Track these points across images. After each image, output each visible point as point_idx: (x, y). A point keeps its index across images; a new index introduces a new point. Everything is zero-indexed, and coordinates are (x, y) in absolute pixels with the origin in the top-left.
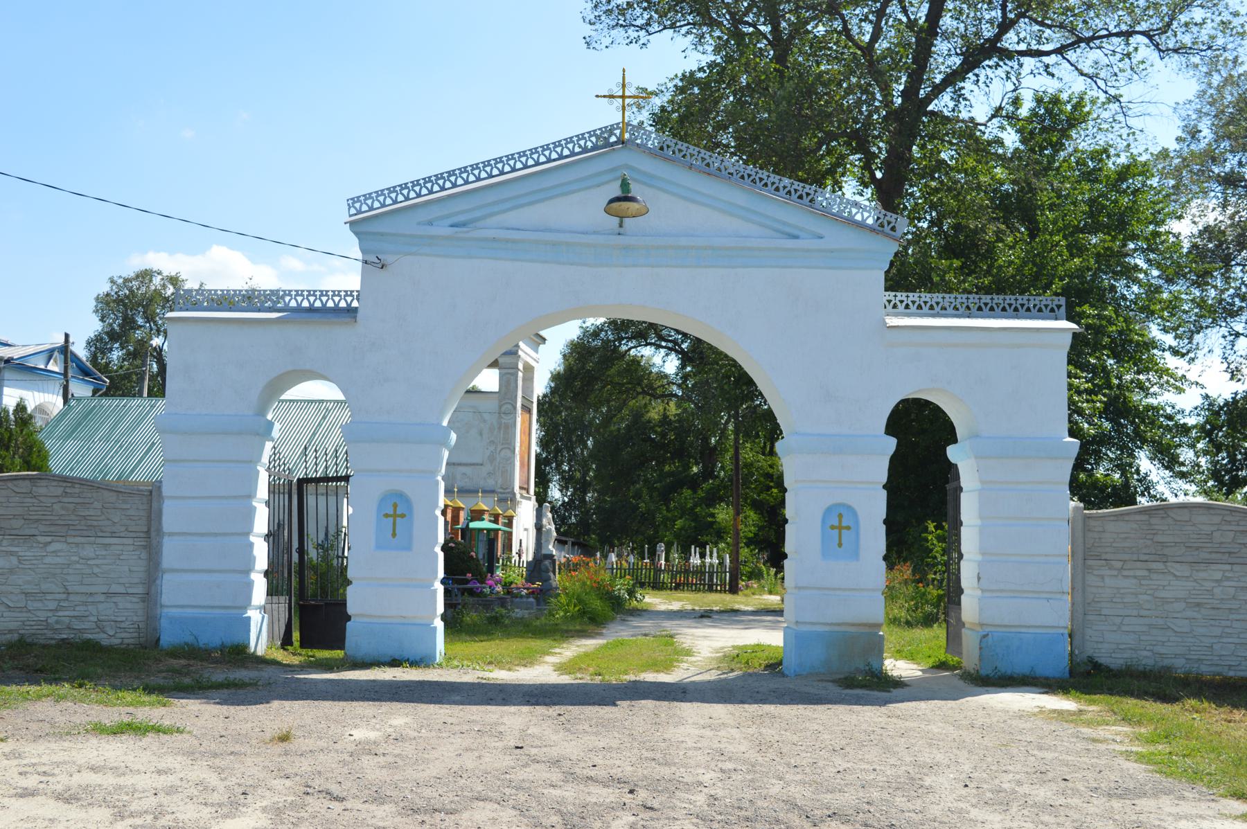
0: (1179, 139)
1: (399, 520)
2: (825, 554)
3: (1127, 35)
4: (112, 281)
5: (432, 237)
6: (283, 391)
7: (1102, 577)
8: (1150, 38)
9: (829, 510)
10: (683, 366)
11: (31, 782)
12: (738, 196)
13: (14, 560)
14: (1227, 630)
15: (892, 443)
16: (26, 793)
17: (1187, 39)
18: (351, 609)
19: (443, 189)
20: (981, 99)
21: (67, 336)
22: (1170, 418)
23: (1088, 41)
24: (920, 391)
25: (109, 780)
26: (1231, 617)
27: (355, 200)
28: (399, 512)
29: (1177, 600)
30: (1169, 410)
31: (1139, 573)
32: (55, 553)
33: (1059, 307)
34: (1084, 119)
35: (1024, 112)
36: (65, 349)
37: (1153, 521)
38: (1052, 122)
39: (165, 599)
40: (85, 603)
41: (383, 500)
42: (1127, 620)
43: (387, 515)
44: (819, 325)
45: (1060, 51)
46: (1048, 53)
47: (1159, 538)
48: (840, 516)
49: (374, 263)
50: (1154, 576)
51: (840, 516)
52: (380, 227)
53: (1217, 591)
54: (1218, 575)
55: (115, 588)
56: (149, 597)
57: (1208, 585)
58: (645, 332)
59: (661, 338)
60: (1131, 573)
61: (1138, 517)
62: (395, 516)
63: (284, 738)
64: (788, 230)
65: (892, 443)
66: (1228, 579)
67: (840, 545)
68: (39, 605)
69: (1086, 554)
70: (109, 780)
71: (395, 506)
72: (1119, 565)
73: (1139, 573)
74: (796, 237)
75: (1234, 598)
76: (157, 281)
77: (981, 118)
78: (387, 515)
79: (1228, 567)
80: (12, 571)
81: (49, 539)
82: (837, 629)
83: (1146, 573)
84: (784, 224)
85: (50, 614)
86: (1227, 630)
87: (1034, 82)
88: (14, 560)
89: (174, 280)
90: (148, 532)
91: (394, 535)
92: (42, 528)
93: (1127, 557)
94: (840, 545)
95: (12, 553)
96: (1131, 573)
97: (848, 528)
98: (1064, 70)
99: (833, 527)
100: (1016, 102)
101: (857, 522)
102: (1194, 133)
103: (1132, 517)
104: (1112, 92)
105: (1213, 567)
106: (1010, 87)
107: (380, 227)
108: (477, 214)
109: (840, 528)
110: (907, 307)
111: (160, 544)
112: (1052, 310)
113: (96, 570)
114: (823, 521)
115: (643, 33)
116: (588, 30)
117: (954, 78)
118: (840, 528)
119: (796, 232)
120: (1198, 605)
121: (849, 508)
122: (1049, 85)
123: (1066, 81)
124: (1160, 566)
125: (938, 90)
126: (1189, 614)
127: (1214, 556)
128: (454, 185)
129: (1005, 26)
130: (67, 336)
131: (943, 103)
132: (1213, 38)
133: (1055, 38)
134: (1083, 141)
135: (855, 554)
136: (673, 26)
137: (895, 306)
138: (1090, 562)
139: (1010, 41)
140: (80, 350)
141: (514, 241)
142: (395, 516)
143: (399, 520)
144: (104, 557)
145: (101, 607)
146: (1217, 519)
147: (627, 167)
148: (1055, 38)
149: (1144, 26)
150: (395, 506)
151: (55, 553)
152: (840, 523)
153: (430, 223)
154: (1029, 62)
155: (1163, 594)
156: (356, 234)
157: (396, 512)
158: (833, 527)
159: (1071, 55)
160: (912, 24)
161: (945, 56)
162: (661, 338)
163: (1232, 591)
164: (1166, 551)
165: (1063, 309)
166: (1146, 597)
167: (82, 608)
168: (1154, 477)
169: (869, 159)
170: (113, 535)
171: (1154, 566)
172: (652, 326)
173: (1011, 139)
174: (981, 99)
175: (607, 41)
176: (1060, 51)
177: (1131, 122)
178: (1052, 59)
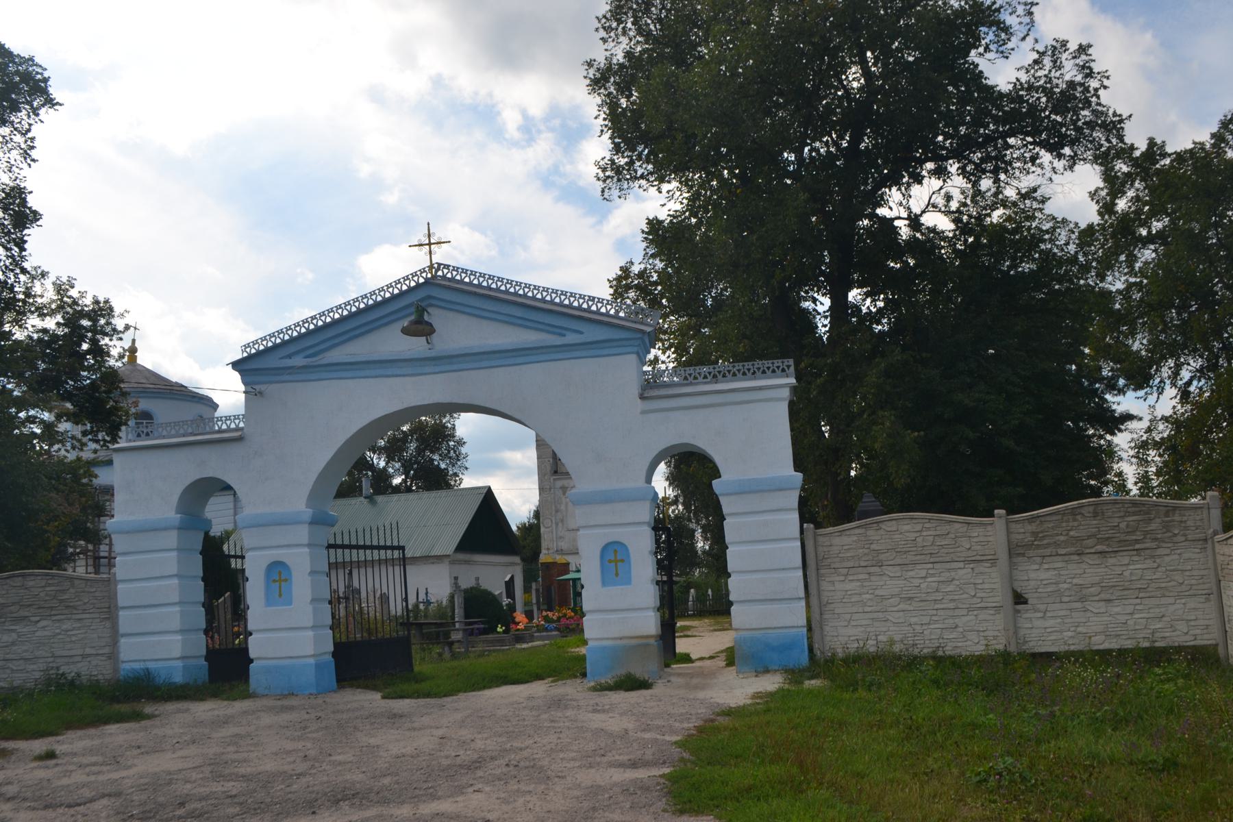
1: (619, 564)
9: (605, 549)
13: (14, 635)
14: (935, 618)
18: (253, 654)
26: (1141, 595)
28: (619, 557)
29: (892, 596)
31: (864, 622)
33: (789, 367)
35: (954, 205)
37: (870, 533)
39: (123, 656)
40: (68, 664)
42: (855, 617)
47: (874, 547)
48: (615, 551)
50: (873, 578)
51: (615, 551)
54: (923, 573)
55: (88, 651)
56: (113, 656)
57: (916, 582)
60: (855, 577)
61: (857, 531)
68: (34, 667)
79: (930, 566)
80: (13, 643)
82: (619, 642)
83: (867, 576)
85: (1128, 617)
86: (935, 618)
91: (280, 595)
93: (850, 564)
94: (617, 575)
96: (855, 577)
97: (622, 561)
99: (610, 561)
101: (628, 556)
103: (852, 532)
105: (918, 567)
110: (715, 376)
112: (783, 370)
114: (602, 556)
120: (910, 599)
126: (902, 606)
137: (715, 376)
138: (1015, 560)
143: (619, 564)
144: (79, 628)
145: (79, 665)
146: (919, 527)
153: (289, 356)
156: (240, 372)
158: (610, 561)
165: (792, 368)
166: (868, 596)
167: (951, 621)
171: (872, 570)
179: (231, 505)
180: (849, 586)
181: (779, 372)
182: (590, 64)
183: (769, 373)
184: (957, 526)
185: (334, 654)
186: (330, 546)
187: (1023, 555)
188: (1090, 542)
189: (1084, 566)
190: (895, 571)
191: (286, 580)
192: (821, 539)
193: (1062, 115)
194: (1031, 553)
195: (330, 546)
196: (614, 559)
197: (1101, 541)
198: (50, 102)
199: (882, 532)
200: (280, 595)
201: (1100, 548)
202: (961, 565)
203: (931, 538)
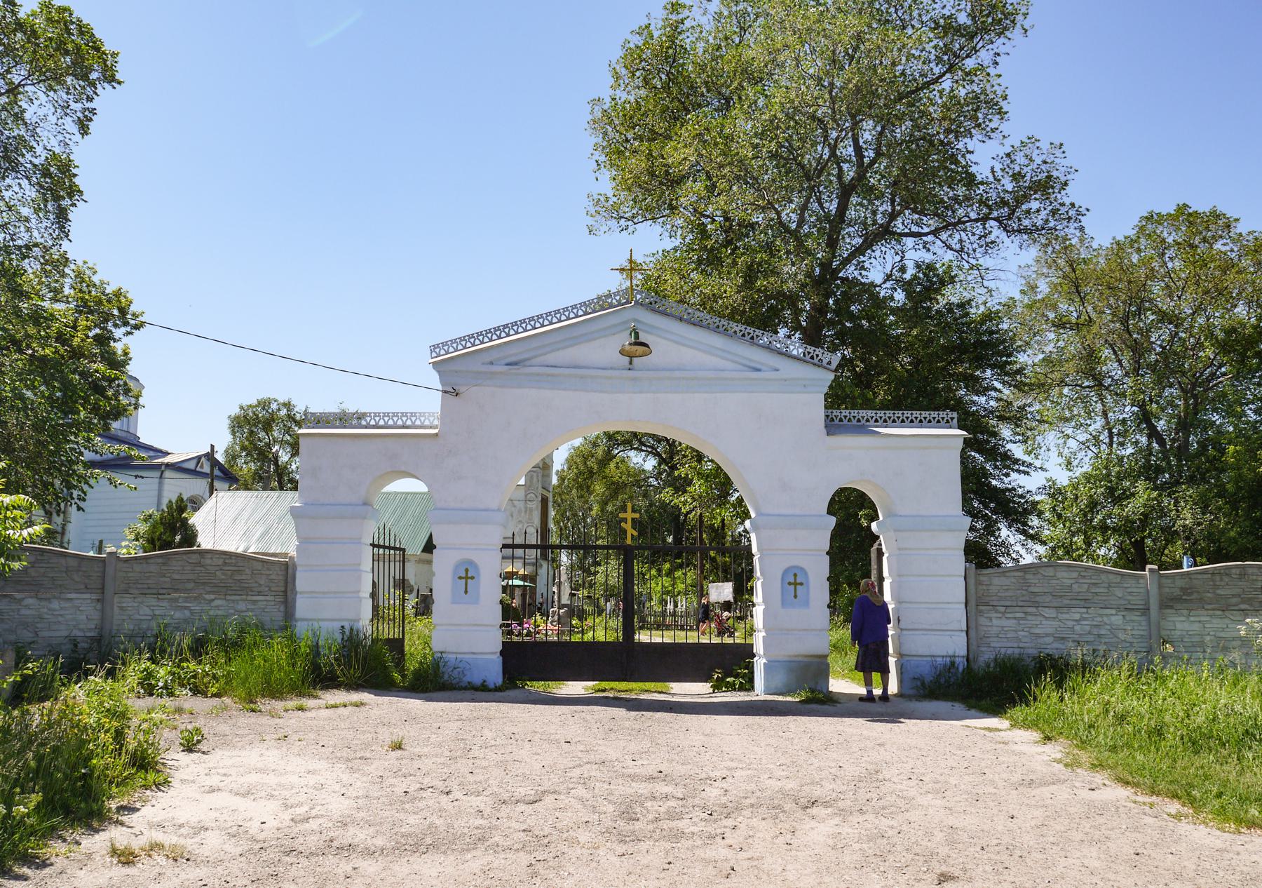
0: (1022, 292)
2: (784, 603)
3: (985, 219)
4: (241, 408)
5: (492, 373)
6: (384, 486)
7: (990, 619)
8: (1000, 222)
10: (659, 465)
11: (214, 781)
12: (717, 341)
13: (187, 613)
15: (832, 521)
16: (212, 790)
17: (1026, 222)
19: (499, 338)
20: (876, 269)
21: (212, 446)
22: (1022, 496)
23: (955, 225)
24: (852, 482)
25: (272, 780)
27: (436, 346)
29: (1047, 635)
30: (1020, 491)
31: (1203, 619)
32: (218, 607)
34: (952, 280)
35: (907, 276)
36: (210, 456)
37: (1028, 576)
38: (929, 282)
41: (457, 567)
43: (460, 578)
44: (767, 430)
45: (935, 233)
46: (926, 235)
47: (1219, 592)
48: (795, 575)
49: (451, 392)
50: (1029, 618)
51: (795, 575)
52: (460, 369)
53: (1077, 628)
54: (1077, 617)
57: (1070, 624)
58: (634, 440)
59: (642, 444)
62: (466, 578)
63: (398, 746)
64: (753, 365)
65: (832, 521)
66: (1085, 619)
67: (795, 596)
69: (975, 603)
70: (272, 780)
71: (467, 570)
72: (1002, 609)
73: (1203, 619)
74: (759, 370)
75: (1090, 633)
76: (274, 406)
77: (878, 281)
78: (460, 578)
81: (212, 597)
84: (750, 360)
87: (915, 254)
88: (187, 613)
89: (288, 405)
90: (285, 592)
91: (466, 592)
92: (208, 589)
94: (795, 596)
95: (186, 608)
97: (801, 584)
98: (938, 247)
99: (790, 584)
100: (903, 270)
102: (1033, 288)
104: (973, 262)
106: (898, 258)
107: (460, 369)
108: (525, 356)
109: (795, 584)
111: (294, 601)
113: (60, 619)
114: (783, 579)
115: (630, 223)
116: (590, 221)
117: (860, 251)
118: (795, 584)
119: (758, 366)
120: (1063, 638)
121: (802, 569)
122: (927, 257)
123: (941, 255)
124: (1033, 610)
125: (846, 262)
127: (1074, 602)
128: (508, 335)
129: (893, 216)
130: (212, 446)
131: (851, 271)
132: (1047, 221)
133: (933, 223)
134: (951, 295)
135: (806, 603)
136: (653, 218)
139: (899, 225)
140: (220, 457)
141: (553, 375)
142: (466, 578)
146: (1075, 575)
147: (635, 320)
148: (933, 223)
149: (995, 214)
150: (467, 570)
151: (28, 607)
152: (794, 582)
153: (492, 363)
154: (909, 242)
155: (1037, 631)
157: (467, 576)
158: (790, 584)
159: (944, 236)
160: (827, 215)
161: (851, 239)
162: (642, 444)
163: (1088, 628)
164: (1038, 599)
165: (955, 421)
168: (1012, 540)
169: (797, 312)
170: (260, 593)
171: (1030, 610)
172: (635, 434)
173: (900, 296)
174: (876, 269)
175: (605, 228)
176: (935, 233)
177: (986, 283)
178: (930, 238)
179: (156, 487)
180: (1004, 623)
181: (907, 422)
182: (1237, 220)
183: (925, 422)
184: (1111, 576)
185: (502, 653)
186: (505, 546)
187: (1171, 607)
188: (1234, 600)
189: (1227, 621)
190: (1050, 613)
191: (472, 578)
192: (982, 578)
193: (1030, 199)
194: (1178, 606)
195: (505, 546)
196: (467, 576)
197: (1244, 601)
198: (110, 78)
199: (1039, 576)
200: (466, 592)
201: (1243, 606)
202: (1113, 612)
203: (1086, 586)
